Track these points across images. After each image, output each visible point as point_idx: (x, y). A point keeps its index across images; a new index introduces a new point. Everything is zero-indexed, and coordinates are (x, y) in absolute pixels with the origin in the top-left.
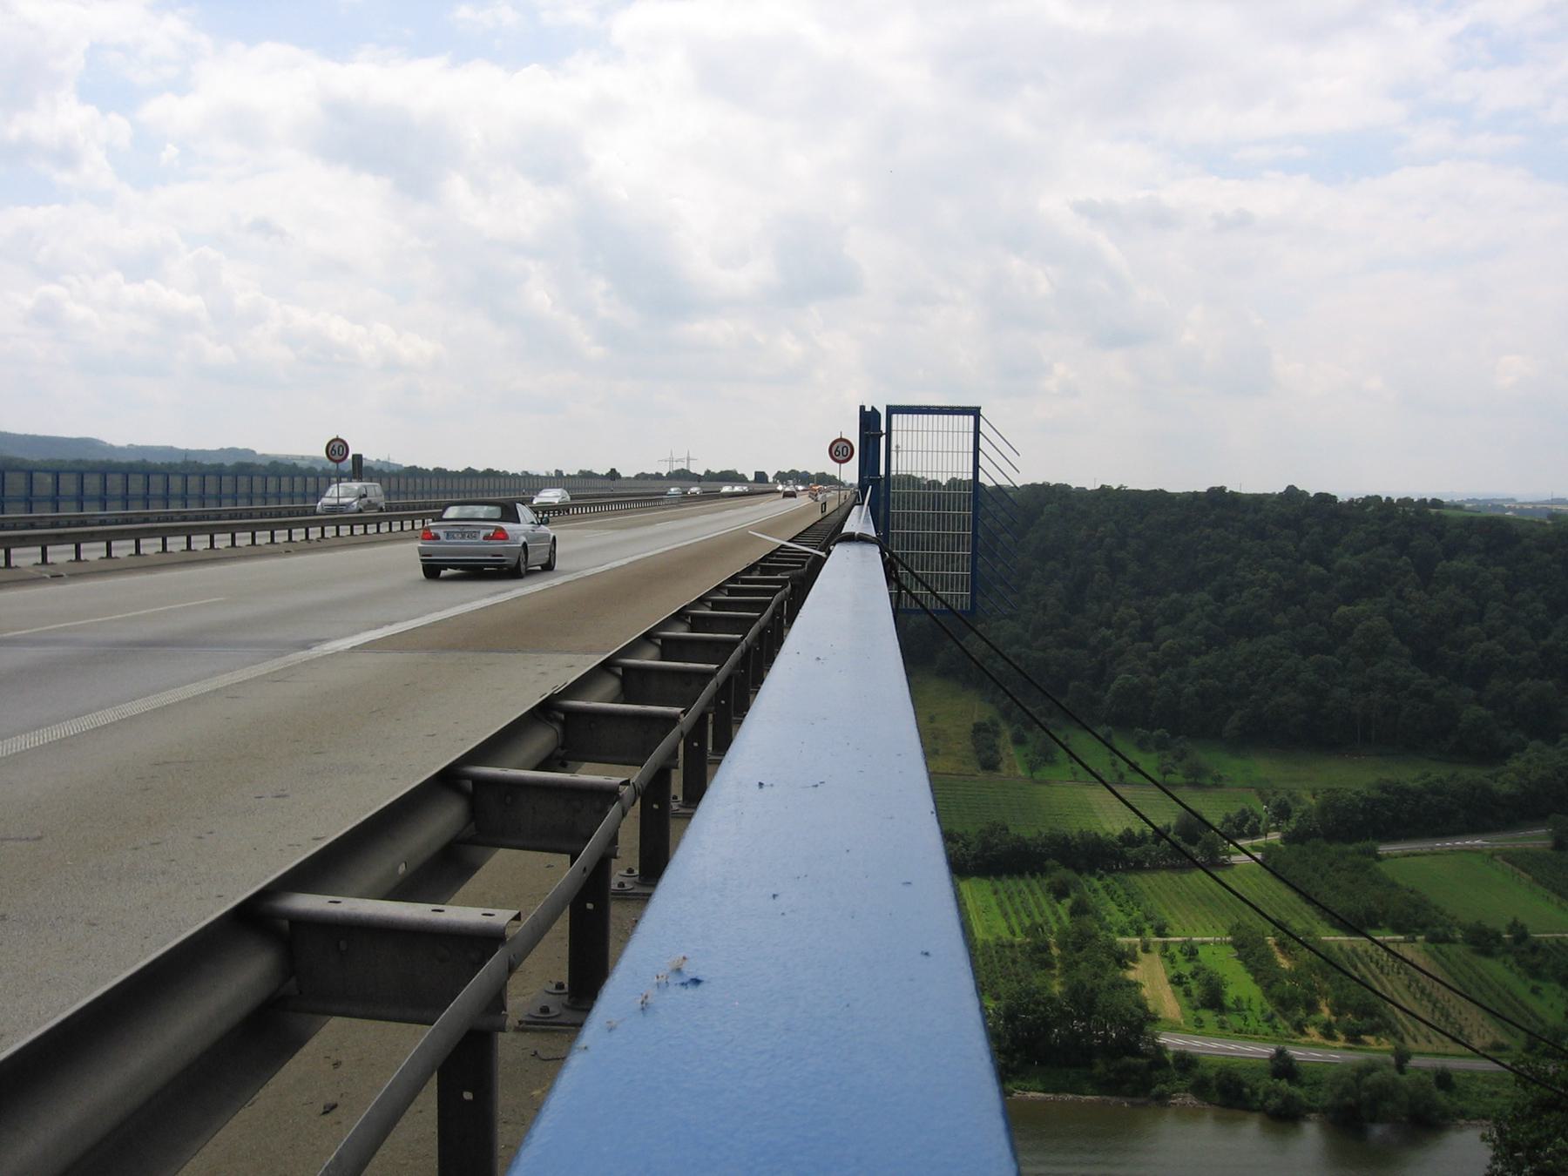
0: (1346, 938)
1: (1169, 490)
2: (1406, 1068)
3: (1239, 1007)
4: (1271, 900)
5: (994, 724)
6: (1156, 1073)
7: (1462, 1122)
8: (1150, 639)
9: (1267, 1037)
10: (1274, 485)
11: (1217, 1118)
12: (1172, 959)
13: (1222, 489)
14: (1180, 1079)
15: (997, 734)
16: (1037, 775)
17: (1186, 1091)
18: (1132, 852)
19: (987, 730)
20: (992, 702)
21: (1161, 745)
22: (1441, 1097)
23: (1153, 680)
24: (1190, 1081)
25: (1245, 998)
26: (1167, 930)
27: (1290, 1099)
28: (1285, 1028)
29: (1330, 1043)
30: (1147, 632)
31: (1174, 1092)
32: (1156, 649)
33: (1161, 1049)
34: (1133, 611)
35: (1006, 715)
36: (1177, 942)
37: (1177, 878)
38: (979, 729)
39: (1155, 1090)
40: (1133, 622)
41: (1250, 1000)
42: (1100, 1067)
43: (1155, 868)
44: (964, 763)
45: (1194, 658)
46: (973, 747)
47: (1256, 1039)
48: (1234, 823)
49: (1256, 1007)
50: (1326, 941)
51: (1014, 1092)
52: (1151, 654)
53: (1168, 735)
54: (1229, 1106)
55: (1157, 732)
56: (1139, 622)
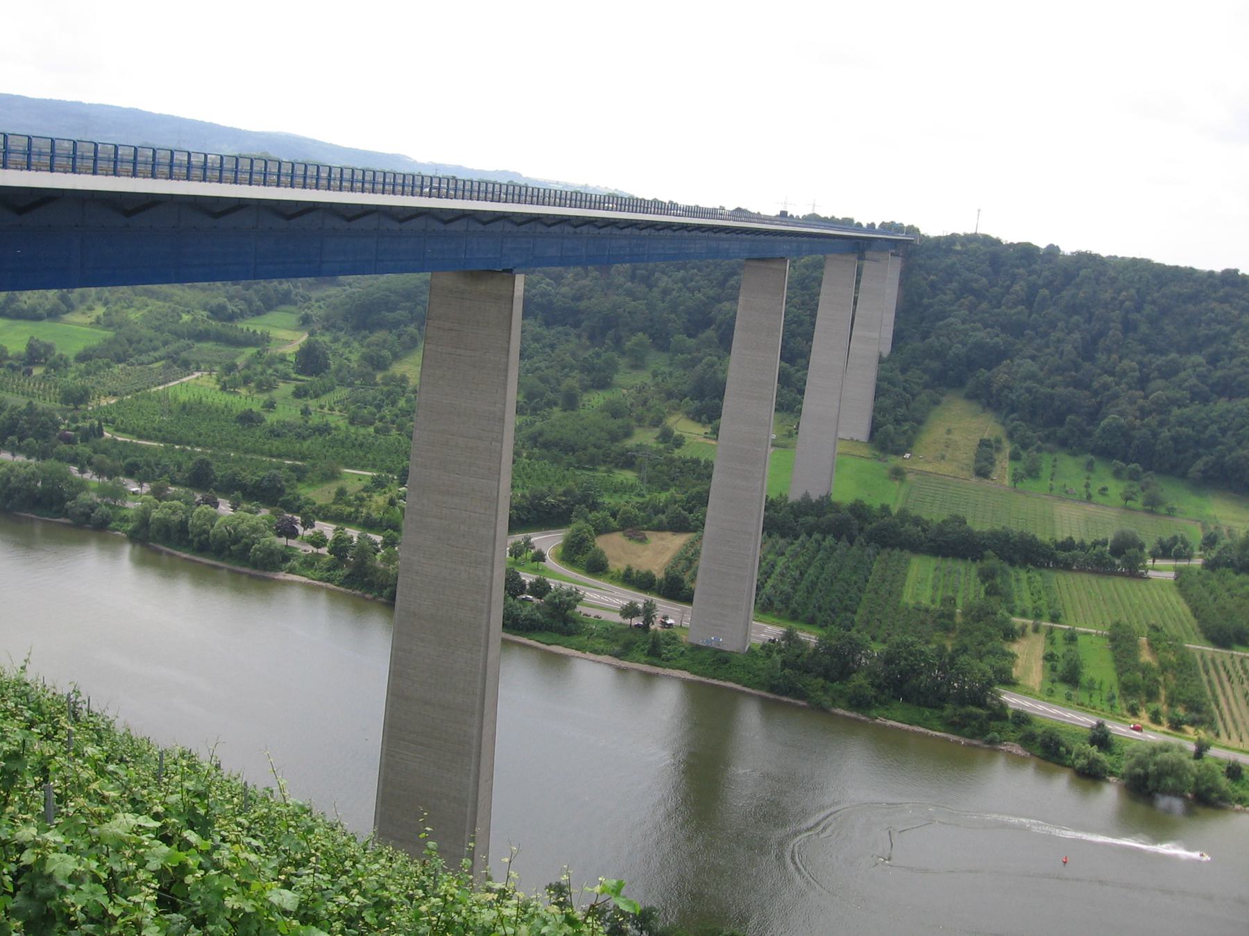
0: (1211, 649)
1: (1167, 264)
2: (1204, 756)
3: (1091, 687)
4: (1165, 609)
5: (998, 441)
6: (992, 723)
7: (1238, 807)
8: (1143, 389)
9: (1102, 713)
10: (494, 170)
11: (1038, 768)
12: (1052, 642)
13: (1236, 271)
14: (1013, 732)
15: (998, 450)
16: (1019, 485)
17: (1015, 741)
18: (1062, 555)
19: (990, 446)
20: (1003, 424)
21: (1134, 476)
22: (1224, 782)
23: (1138, 422)
24: (1020, 735)
25: (1098, 680)
26: (1061, 619)
27: (1094, 762)
28: (1122, 708)
29: (1154, 727)
30: (1143, 382)
31: (1005, 741)
32: (1146, 397)
33: (1003, 706)
34: (1134, 364)
35: (1010, 436)
36: (1064, 629)
37: (1094, 582)
38: (984, 443)
39: (989, 736)
40: (1132, 374)
41: (1101, 683)
42: (949, 710)
43: (1081, 570)
44: (962, 469)
45: (1176, 408)
46: (974, 457)
47: (1092, 713)
48: (574, 453)
49: (1105, 687)
50: (1188, 648)
51: (877, 718)
52: (1140, 401)
53: (1140, 469)
54: (1046, 759)
55: (1132, 466)
56: (1137, 374)
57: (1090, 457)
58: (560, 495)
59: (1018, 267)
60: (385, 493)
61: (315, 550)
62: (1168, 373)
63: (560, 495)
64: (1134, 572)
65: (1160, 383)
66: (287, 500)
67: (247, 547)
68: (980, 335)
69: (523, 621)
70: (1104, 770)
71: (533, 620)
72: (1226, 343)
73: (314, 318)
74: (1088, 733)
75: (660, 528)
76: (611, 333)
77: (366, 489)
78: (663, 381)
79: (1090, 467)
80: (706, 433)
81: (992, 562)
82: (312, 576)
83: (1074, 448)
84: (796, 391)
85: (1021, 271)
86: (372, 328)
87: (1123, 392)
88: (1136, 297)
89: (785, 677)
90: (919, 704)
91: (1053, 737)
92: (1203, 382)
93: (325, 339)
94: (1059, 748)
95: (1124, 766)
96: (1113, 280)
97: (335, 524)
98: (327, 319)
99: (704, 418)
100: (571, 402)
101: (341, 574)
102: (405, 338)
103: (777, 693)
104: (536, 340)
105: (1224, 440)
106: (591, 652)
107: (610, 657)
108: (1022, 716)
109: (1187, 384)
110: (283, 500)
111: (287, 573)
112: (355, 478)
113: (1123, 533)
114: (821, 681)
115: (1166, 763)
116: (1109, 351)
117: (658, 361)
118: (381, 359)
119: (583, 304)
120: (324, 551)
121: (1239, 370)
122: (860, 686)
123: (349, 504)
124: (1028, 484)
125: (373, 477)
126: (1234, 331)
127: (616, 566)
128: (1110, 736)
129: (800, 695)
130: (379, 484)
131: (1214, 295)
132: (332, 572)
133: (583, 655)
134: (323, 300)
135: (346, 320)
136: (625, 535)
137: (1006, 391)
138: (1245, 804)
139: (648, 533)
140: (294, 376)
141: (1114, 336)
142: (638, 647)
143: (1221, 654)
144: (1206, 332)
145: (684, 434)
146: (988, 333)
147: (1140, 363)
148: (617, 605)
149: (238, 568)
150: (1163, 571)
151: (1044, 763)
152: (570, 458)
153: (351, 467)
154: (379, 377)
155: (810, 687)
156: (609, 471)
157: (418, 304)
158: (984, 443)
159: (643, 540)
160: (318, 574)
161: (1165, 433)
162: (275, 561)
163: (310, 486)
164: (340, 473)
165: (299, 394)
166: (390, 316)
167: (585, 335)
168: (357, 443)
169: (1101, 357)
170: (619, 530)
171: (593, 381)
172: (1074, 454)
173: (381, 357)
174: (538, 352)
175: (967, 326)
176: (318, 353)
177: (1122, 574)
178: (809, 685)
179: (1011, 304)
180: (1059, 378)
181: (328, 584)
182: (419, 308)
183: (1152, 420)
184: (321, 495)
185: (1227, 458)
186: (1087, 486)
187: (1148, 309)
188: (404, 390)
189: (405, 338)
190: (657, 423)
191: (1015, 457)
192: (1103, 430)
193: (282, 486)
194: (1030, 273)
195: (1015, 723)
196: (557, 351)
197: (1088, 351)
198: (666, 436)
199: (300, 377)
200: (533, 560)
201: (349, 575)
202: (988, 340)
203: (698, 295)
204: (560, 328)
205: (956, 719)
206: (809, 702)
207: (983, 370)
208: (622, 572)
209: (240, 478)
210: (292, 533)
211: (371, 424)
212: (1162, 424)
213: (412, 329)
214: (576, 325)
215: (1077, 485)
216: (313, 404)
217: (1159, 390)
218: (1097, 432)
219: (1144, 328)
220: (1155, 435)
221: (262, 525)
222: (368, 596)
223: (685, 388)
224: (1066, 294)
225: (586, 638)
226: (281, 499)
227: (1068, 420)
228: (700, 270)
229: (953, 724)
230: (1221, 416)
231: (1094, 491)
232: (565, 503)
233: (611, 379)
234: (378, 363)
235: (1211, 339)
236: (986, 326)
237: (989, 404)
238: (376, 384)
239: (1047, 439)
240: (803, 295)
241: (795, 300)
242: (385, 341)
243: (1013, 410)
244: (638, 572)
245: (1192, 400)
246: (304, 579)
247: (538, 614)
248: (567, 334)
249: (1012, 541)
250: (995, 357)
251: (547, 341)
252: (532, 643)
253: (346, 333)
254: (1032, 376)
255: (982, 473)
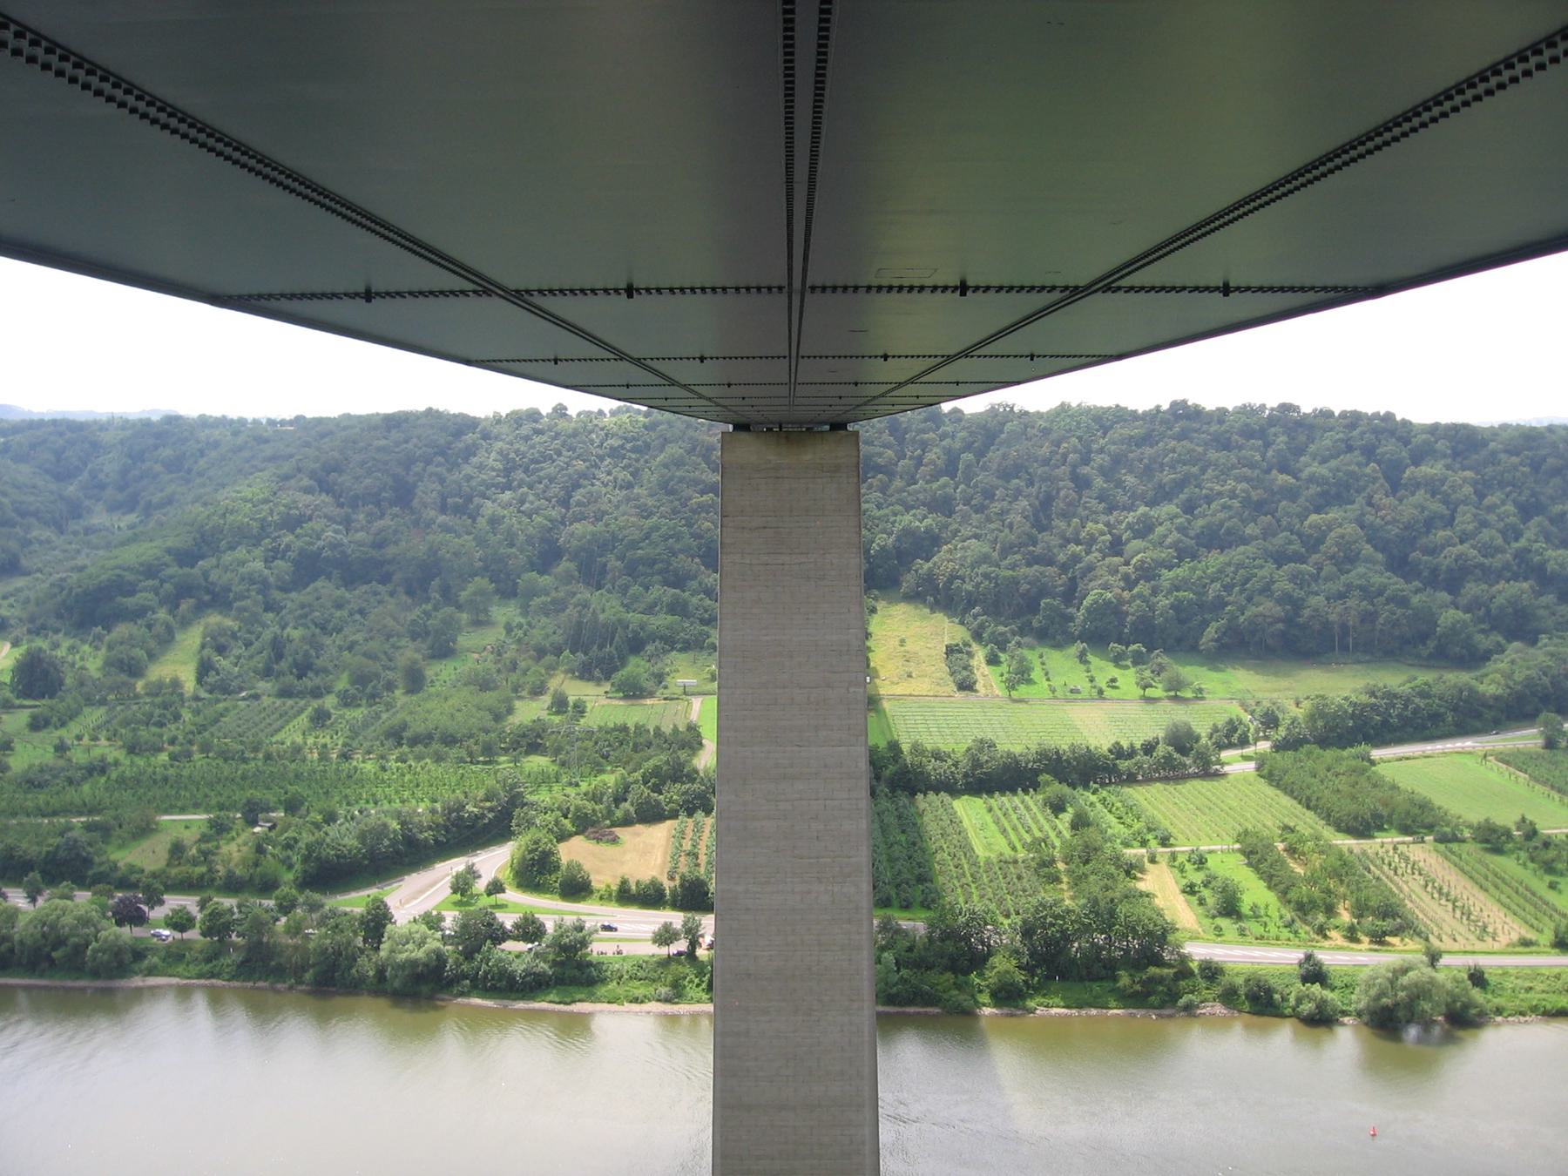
0: (1355, 842)
7: (1499, 1019)
11: (1247, 1027)
14: (1208, 989)
18: (1124, 765)
23: (1126, 594)
26: (1172, 841)
30: (1116, 547)
34: (1101, 526)
37: (1172, 789)
39: (1182, 1002)
43: (1148, 780)
50: (1336, 845)
52: (1123, 569)
56: (1108, 537)
57: (1080, 646)
58: (481, 801)
59: (924, 431)
60: (233, 839)
61: (178, 935)
62: (1144, 529)
63: (481, 801)
64: (1208, 772)
65: (1136, 544)
66: (101, 873)
67: (80, 949)
68: (906, 519)
69: (523, 978)
70: (1482, 1014)
71: (539, 975)
72: (1199, 486)
73: (12, 622)
74: (1296, 970)
75: (627, 822)
76: (435, 583)
77: (204, 838)
78: (525, 635)
79: (1082, 658)
80: (606, 692)
81: (1057, 788)
82: (187, 974)
83: (1058, 637)
84: (698, 621)
85: (931, 435)
86: (108, 622)
87: (1099, 561)
88: (1080, 447)
89: (903, 980)
90: (1081, 979)
91: (1262, 984)
92: (1186, 536)
93: (41, 643)
94: (1272, 997)
95: (1359, 1000)
96: (1046, 432)
97: (196, 895)
98: (32, 620)
99: (597, 673)
100: (415, 681)
101: (229, 961)
102: (159, 629)
103: (900, 1005)
104: (339, 606)
105: (1231, 599)
106: (631, 1002)
107: (659, 1004)
108: (1214, 966)
109: (1169, 540)
110: (95, 874)
111: (146, 976)
112: (186, 824)
113: (1175, 726)
114: (949, 975)
115: (1416, 985)
116: (1065, 516)
117: (504, 613)
118: (133, 662)
119: (391, 551)
120: (193, 934)
121: (1221, 516)
122: (1007, 972)
123: (195, 863)
124: (1023, 690)
125: (210, 820)
126: (1203, 471)
127: (599, 882)
128: (1324, 968)
129: (930, 1000)
130: (219, 829)
131: (1169, 432)
132: (214, 962)
133: (620, 1008)
134: (12, 595)
135: (59, 616)
136: (588, 838)
137: (957, 583)
138: (1505, 1014)
139: (618, 831)
140: (17, 702)
141: (1067, 497)
142: (691, 981)
143: (1365, 844)
144: (1173, 476)
145: (584, 698)
146: (914, 515)
147: (1107, 524)
148: (645, 932)
149: (69, 983)
150: (1236, 764)
151: (1255, 1019)
152: (454, 752)
153: (166, 812)
154: (140, 685)
155: (939, 987)
156: (515, 761)
157: (165, 581)
158: (950, 650)
159: (615, 840)
160: (194, 969)
161: (1163, 602)
162: (127, 961)
163: (121, 847)
164: (157, 824)
165: (37, 725)
166: (130, 602)
167: (400, 589)
168: (158, 777)
169: (1060, 524)
170: (577, 833)
171: (431, 648)
172: (1058, 646)
173: (133, 658)
174: (346, 622)
175: (886, 511)
176: (45, 665)
177: (1195, 776)
178: (938, 984)
179: (928, 477)
180: (1018, 557)
181: (214, 981)
182: (167, 586)
183: (1142, 588)
184: (145, 857)
185: (1242, 619)
186: (1092, 680)
187: (1098, 459)
188: (182, 701)
189: (159, 629)
190: (538, 691)
191: (993, 661)
192: (1088, 610)
193: (89, 853)
194: (943, 437)
195: (1205, 977)
196: (372, 617)
197: (1041, 517)
198: (560, 704)
199: (27, 702)
200: (489, 893)
201: (242, 962)
202: (917, 523)
203: (538, 519)
204: (365, 588)
205: (1138, 987)
206: (943, 1008)
207: (919, 561)
208: (614, 888)
209: (21, 853)
210: (139, 919)
211: (161, 750)
212: (1155, 592)
213: (162, 614)
214: (385, 579)
215: (1078, 679)
216: (67, 734)
217: (1140, 551)
218: (1080, 615)
219: (1099, 482)
220: (1152, 608)
221: (94, 913)
222: (279, 986)
223: (557, 639)
224: (994, 455)
225: (615, 983)
226: (90, 873)
227: (1042, 604)
228: (531, 487)
229: (1135, 995)
230: (1220, 571)
231: (1102, 682)
232: (491, 810)
233: (454, 641)
234: (133, 669)
235: (1181, 485)
236: (908, 508)
237: (937, 602)
238: (137, 696)
239: (1022, 632)
240: (672, 502)
241: (662, 508)
242: (131, 637)
243: (971, 604)
244: (638, 883)
245: (1181, 559)
246: (174, 980)
247: (542, 964)
248: (376, 593)
249: (1065, 758)
250: (927, 544)
251: (354, 606)
252: (544, 1005)
253: (65, 634)
254: (985, 559)
255: (966, 686)
